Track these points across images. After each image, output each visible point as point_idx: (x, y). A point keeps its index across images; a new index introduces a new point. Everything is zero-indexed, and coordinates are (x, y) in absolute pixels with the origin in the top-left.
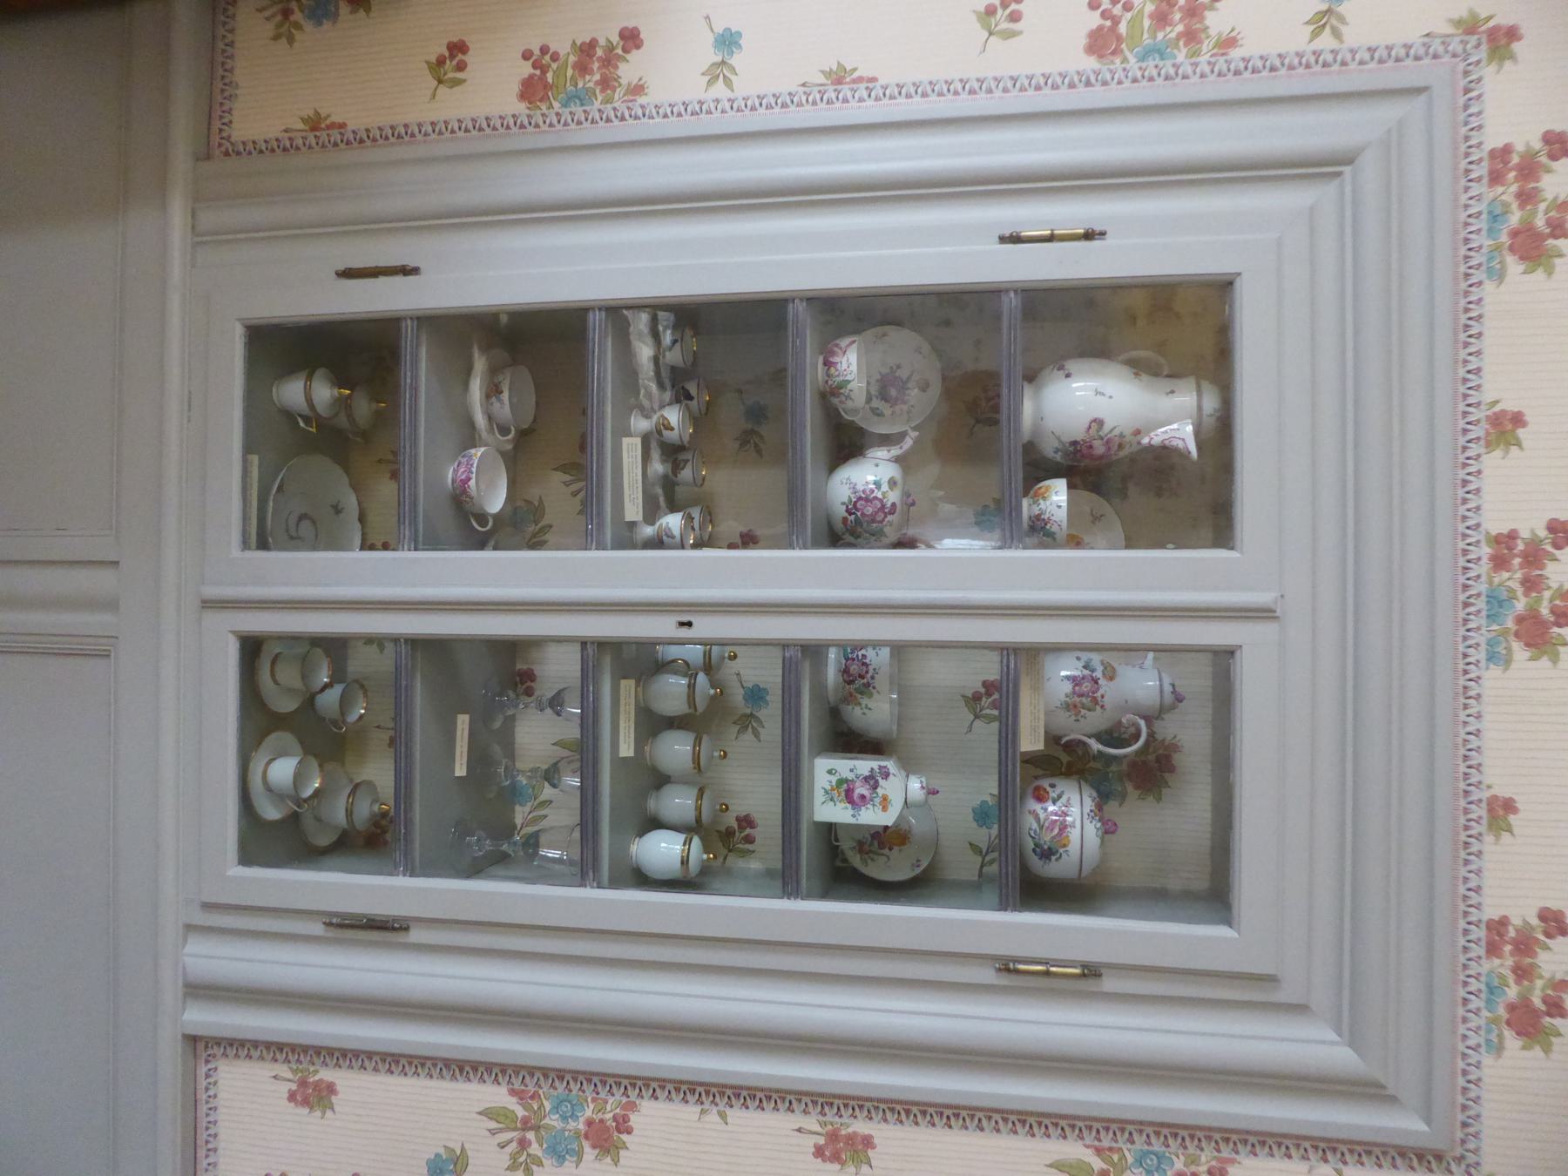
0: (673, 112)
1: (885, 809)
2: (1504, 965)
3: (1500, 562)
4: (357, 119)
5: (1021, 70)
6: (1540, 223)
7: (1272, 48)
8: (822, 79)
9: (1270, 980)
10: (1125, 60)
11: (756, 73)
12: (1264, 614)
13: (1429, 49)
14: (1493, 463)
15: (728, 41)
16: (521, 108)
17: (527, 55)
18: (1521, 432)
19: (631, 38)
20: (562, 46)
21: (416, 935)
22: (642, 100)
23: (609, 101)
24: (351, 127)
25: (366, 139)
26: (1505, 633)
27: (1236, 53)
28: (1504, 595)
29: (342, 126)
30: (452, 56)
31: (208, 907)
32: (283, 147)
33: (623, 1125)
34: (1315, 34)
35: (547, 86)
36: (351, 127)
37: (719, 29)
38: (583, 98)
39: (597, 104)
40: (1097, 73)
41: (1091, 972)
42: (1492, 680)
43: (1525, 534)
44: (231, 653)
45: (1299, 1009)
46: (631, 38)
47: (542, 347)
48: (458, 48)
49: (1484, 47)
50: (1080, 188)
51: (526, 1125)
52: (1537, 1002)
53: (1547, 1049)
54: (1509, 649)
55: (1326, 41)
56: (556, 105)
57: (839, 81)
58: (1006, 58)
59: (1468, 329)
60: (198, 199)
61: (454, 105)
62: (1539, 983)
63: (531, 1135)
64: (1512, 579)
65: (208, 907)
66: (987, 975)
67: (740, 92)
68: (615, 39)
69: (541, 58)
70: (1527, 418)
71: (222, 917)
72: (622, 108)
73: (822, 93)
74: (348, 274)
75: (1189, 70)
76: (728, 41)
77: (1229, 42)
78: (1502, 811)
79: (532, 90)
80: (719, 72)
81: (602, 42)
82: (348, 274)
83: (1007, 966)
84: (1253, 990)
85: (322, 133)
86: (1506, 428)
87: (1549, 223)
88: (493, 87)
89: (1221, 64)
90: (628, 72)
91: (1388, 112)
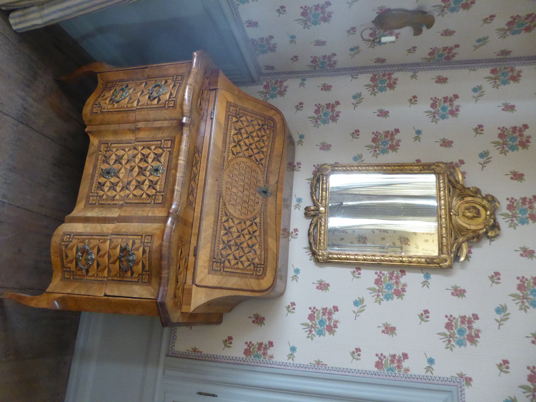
1: (360, 156)
5: (360, 368)
6: (454, 109)
7: (417, 373)
8: (314, 363)
10: (384, 370)
13: (452, 379)
15: (293, 349)
16: (244, 356)
17: (246, 343)
18: (465, 294)
20: (255, 343)
22: (272, 360)
23: (265, 358)
24: (203, 353)
26: (464, 339)
27: (409, 373)
28: (464, 330)
29: (201, 352)
30: (229, 340)
34: (427, 371)
35: (250, 352)
36: (203, 353)
37: (291, 346)
38: (258, 356)
39: (262, 359)
40: (377, 372)
43: (467, 316)
48: (230, 338)
49: (465, 382)
51: (379, 291)
52: (473, 334)
53: (476, 345)
54: (466, 342)
55: (429, 374)
56: (252, 357)
57: (318, 364)
58: (357, 365)
62: (473, 330)
63: (380, 294)
67: (295, 362)
68: (267, 343)
69: (250, 345)
70: (473, 379)
72: (268, 361)
73: (314, 366)
74: (200, 393)
75: (398, 375)
77: (407, 370)
79: (247, 352)
80: (291, 356)
81: (264, 343)
82: (200, 393)
85: (196, 356)
87: (475, 334)
88: (237, 350)
89: (405, 376)
90: (270, 352)
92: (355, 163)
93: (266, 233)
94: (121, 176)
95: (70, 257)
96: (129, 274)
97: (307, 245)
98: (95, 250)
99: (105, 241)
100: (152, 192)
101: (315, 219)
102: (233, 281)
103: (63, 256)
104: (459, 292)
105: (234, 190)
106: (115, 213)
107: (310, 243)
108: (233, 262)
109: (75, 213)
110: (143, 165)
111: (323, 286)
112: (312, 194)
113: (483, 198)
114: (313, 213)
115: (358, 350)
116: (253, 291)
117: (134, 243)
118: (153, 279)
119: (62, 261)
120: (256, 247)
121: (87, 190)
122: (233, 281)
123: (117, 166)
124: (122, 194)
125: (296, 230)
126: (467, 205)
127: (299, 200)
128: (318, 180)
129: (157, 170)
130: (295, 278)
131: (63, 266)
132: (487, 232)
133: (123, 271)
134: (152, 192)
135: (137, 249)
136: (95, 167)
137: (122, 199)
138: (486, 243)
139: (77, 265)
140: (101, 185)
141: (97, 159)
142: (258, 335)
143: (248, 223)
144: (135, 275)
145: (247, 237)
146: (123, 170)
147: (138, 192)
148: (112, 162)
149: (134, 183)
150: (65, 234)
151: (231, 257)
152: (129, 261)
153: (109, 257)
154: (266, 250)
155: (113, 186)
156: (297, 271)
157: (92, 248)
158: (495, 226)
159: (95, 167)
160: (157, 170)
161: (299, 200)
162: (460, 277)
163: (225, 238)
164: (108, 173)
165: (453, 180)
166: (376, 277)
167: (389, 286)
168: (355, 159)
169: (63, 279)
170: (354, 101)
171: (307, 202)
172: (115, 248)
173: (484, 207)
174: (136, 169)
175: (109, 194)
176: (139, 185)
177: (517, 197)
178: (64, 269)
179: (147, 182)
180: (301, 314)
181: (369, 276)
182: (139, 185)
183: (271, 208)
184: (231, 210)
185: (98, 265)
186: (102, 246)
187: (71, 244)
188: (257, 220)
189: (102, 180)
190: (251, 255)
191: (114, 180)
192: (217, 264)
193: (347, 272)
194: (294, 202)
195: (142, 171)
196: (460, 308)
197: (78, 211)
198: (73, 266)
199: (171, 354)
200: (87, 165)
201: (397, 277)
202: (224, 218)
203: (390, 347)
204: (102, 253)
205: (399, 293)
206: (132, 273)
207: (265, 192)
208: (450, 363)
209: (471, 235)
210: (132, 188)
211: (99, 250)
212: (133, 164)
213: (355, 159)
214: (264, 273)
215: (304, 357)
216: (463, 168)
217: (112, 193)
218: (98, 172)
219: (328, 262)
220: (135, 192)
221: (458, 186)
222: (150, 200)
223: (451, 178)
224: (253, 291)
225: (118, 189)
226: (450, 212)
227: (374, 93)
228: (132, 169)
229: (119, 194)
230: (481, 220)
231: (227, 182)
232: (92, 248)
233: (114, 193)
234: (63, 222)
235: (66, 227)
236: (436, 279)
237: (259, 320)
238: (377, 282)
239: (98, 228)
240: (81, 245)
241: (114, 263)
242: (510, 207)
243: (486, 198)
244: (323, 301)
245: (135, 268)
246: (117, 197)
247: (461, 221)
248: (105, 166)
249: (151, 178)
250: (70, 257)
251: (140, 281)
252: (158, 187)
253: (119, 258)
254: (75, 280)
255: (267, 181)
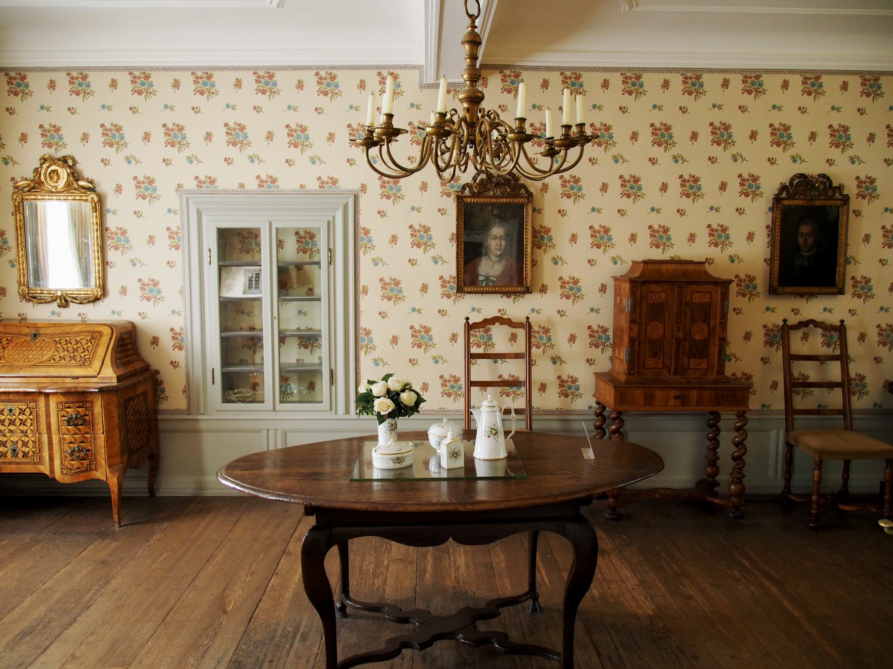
0: (186, 322)
1: (11, 261)
2: (326, 186)
3: (263, 186)
4: (184, 383)
9: (329, 222)
11: (180, 307)
12: (270, 224)
14: (247, 187)
15: (173, 312)
19: (172, 330)
20: (172, 343)
21: (333, 368)
25: (188, 381)
31: (331, 409)
32: (189, 398)
33: (365, 329)
41: (330, 250)
42: (281, 188)
44: (283, 405)
45: (334, 217)
46: (172, 330)
47: (227, 345)
48: (172, 363)
50: (335, 339)
58: (179, 263)
59: (226, 192)
60: (199, 413)
61: (182, 364)
64: (265, 185)
65: (331, 409)
66: (332, 267)
71: (332, 407)
76: (173, 312)
78: (302, 186)
79: (180, 348)
80: (179, 314)
83: (330, 263)
84: (330, 225)
85: (187, 390)
86: (241, 186)
90: (178, 330)
91: (191, 203)
92: (17, 266)
93: (69, 333)
94: (16, 439)
95: (79, 465)
96: (87, 418)
97: (91, 305)
98: (72, 445)
99: (64, 439)
100: (28, 412)
101: (68, 299)
102: (101, 352)
103: (80, 471)
104: (119, 189)
105: (31, 357)
106: (45, 437)
107: (89, 302)
108: (86, 353)
109: (47, 472)
110: (7, 422)
111: (124, 291)
112: (46, 303)
113: (41, 167)
114: (63, 301)
115: (589, 261)
116: (111, 339)
117: (64, 416)
118: (89, 399)
119: (82, 472)
120: (78, 339)
121: (29, 466)
122: (101, 352)
123: (9, 444)
124: (30, 435)
125: (80, 315)
126: (48, 179)
127: (53, 313)
128: (35, 297)
129: (11, 410)
130: (119, 314)
131: (86, 471)
132: (70, 167)
133: (85, 423)
134: (28, 412)
135: (68, 412)
136: (10, 463)
137: (34, 435)
138: (79, 167)
139: (84, 459)
140: (25, 455)
141: (4, 463)
142: (166, 341)
143: (59, 345)
144: (87, 413)
145: (69, 345)
146: (12, 439)
147: (29, 423)
148: (6, 449)
149: (22, 428)
150: (62, 473)
151: (82, 355)
152: (76, 418)
153: (76, 434)
154: (82, 332)
155: (25, 444)
156: (113, 312)
157: (70, 447)
158: (64, 160)
159: (10, 463)
160: (11, 410)
161: (53, 313)
162: (105, 186)
163: (67, 359)
164: (14, 450)
165: (27, 189)
166: (112, 249)
167: (119, 240)
168: (13, 266)
169: (96, 469)
170: (559, 363)
171: (54, 306)
172: (68, 430)
173: (48, 167)
174: (11, 427)
175: (31, 446)
176: (23, 423)
177: (41, 140)
178: (89, 469)
179: (21, 417)
180: (147, 307)
181: (111, 255)
182: (23, 423)
183: (48, 331)
184: (46, 357)
185: (82, 442)
186: (68, 441)
187: (69, 466)
188: (57, 339)
189: (21, 455)
190: (84, 342)
191: (20, 444)
192: (85, 363)
193: (110, 272)
194: (55, 317)
195: (12, 423)
196: (130, 188)
197: (45, 469)
198: (85, 462)
199: (189, 411)
200: (8, 471)
201: (112, 233)
202: (52, 361)
203: (163, 240)
204: (73, 440)
205: (124, 233)
206: (86, 415)
207: (35, 335)
208: (169, 197)
209: (71, 178)
210: (25, 428)
211: (71, 443)
212: (7, 431)
213: (13, 266)
214: (99, 332)
215: (179, 303)
216: (18, 179)
217: (31, 444)
218: (14, 460)
219: (104, 288)
220: (29, 425)
221: (32, 185)
222: (34, 412)
223: (26, 190)
224: (111, 339)
225: (27, 439)
226: (51, 192)
227: (126, 145)
228: (11, 431)
229: (31, 437)
230: (60, 170)
231: (24, 362)
232: (70, 447)
233: (30, 442)
234: (54, 479)
235: (58, 475)
236: (110, 204)
237: (155, 341)
238: (117, 248)
239: (56, 447)
240: (69, 458)
241: (80, 430)
242: (50, 146)
243: (42, 164)
244: (135, 291)
245: (82, 414)
246: (33, 439)
247: (61, 184)
248: (9, 454)
249: (17, 414)
250: (79, 465)
251: (92, 409)
252: (24, 407)
253: (76, 425)
254: (96, 458)
255: (27, 335)
